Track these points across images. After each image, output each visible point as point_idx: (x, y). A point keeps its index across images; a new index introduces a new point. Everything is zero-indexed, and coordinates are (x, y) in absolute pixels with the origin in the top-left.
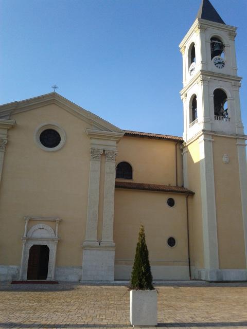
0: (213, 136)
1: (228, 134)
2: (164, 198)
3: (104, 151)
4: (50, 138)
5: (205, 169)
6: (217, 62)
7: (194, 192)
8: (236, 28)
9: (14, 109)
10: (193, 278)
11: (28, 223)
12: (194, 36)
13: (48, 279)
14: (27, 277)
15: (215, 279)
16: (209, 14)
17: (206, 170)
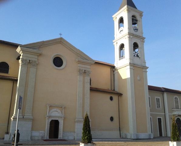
0: (133, 66)
1: (141, 66)
2: (108, 96)
3: (30, 60)
4: (58, 62)
5: (130, 83)
6: (135, 28)
7: (122, 93)
8: (143, 12)
9: (42, 45)
10: (121, 137)
11: (49, 107)
12: (124, 13)
13: (59, 138)
14: (49, 137)
15: (135, 138)
16: (130, 3)
17: (131, 83)
